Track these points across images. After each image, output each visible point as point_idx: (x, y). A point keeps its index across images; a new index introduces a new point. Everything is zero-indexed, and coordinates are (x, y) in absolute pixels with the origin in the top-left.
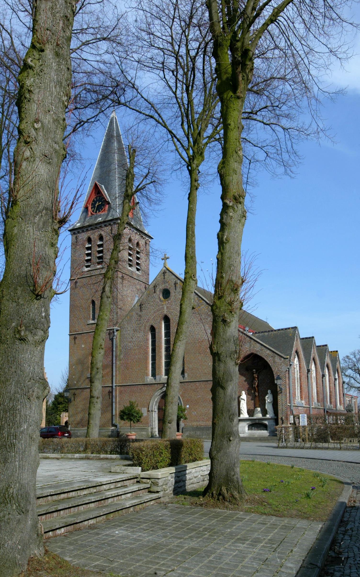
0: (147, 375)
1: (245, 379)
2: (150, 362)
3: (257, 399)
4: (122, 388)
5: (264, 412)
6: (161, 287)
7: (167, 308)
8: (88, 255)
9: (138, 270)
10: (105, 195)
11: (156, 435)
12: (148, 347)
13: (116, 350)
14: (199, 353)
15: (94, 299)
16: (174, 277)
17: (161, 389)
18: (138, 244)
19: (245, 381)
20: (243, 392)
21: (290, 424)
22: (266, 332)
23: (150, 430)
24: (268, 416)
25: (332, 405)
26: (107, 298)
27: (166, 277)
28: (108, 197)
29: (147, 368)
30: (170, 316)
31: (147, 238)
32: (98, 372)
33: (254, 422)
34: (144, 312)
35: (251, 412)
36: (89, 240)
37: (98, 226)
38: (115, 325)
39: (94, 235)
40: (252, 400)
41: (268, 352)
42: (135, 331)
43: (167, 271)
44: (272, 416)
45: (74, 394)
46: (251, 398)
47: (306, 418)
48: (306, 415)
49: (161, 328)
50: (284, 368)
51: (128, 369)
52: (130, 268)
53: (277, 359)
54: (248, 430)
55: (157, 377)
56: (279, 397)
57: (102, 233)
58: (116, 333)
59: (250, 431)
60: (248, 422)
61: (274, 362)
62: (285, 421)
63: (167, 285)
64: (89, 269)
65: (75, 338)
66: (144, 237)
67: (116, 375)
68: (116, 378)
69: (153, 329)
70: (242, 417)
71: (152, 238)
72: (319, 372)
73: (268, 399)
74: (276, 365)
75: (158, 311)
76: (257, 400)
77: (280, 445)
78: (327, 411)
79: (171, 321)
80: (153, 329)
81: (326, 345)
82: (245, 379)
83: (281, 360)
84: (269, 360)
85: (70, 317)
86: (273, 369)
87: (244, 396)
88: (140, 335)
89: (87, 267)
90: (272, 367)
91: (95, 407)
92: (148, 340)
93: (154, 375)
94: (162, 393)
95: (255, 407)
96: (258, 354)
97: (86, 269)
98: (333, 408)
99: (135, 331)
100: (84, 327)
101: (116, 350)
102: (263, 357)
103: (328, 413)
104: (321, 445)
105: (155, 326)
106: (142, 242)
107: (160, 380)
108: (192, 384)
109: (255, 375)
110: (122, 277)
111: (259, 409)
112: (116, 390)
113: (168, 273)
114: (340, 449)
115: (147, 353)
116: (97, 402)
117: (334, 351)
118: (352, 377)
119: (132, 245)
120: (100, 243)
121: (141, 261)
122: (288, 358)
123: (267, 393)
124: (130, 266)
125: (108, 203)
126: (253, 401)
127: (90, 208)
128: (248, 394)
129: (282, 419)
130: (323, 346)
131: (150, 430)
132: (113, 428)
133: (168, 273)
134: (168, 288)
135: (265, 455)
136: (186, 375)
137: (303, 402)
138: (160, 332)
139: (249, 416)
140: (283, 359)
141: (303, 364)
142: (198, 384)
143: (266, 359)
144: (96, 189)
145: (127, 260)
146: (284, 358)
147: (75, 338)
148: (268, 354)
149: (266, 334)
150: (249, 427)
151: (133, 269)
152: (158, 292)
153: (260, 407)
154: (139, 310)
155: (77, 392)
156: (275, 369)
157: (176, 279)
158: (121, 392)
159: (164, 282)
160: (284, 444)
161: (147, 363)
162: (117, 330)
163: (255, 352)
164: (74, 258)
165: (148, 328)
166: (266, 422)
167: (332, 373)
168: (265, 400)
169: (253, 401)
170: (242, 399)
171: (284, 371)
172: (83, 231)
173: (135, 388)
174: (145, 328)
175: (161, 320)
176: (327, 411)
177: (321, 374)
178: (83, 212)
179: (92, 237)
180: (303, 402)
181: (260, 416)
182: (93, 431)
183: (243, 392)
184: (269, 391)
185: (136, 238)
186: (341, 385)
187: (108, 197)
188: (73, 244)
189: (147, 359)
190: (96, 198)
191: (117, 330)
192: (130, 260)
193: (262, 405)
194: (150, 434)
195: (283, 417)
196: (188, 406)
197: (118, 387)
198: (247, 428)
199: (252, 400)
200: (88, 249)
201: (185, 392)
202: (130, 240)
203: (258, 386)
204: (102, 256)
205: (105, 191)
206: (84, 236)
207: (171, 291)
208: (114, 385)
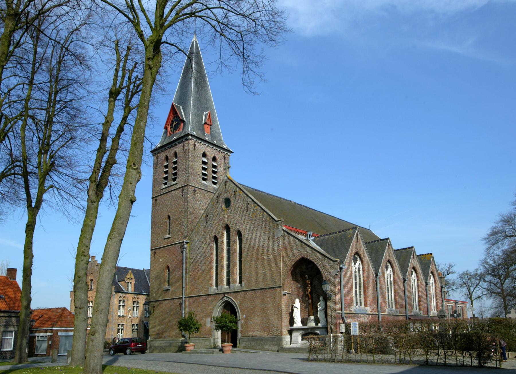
0: (211, 285)
1: (299, 286)
2: (215, 273)
3: (311, 306)
4: (191, 299)
5: (317, 321)
6: (223, 197)
7: (228, 217)
8: (166, 172)
9: (214, 183)
10: (181, 114)
11: (218, 346)
12: (212, 257)
13: (186, 262)
14: (255, 261)
15: (170, 214)
16: (234, 185)
17: (222, 299)
18: (214, 159)
19: (300, 288)
20: (297, 300)
21: (342, 333)
22: (327, 235)
23: (212, 341)
24: (319, 325)
25: (422, 312)
26: (92, 202)
27: (227, 186)
28: (184, 116)
29: (210, 278)
30: (230, 225)
31: (226, 153)
32: (79, 281)
33: (306, 332)
34: (209, 223)
35: (304, 321)
36: (167, 159)
37: (173, 144)
38: (185, 238)
39: (170, 153)
40: (306, 307)
41: (318, 255)
42: (201, 242)
43: (228, 180)
44: (323, 324)
45: (154, 307)
46: (305, 305)
47: (358, 326)
48: (357, 323)
50: (333, 272)
51: (195, 281)
52: (203, 182)
53: (326, 262)
54: (302, 340)
55: (219, 287)
56: (329, 304)
57: (177, 150)
58: (185, 246)
59: (303, 342)
60: (301, 332)
61: (324, 266)
62: (334, 330)
63: (228, 193)
64: (166, 186)
65: (155, 253)
66: (222, 151)
67: (186, 287)
68: (186, 290)
69: (216, 239)
71: (232, 152)
72: (399, 277)
73: (320, 306)
74: (327, 269)
75: (220, 220)
76: (310, 308)
77: (311, 358)
78: (409, 318)
79: (231, 230)
80: (216, 239)
81: (412, 247)
82: (299, 286)
83: (330, 263)
84: (319, 264)
85: (151, 234)
86: (323, 274)
87: (297, 304)
88: (205, 246)
89: (165, 184)
90: (321, 271)
91: (78, 318)
92: (212, 250)
93: (228, 283)
94: (223, 303)
95: (309, 316)
96: (308, 258)
97: (164, 187)
98: (422, 315)
99: (201, 242)
100: (161, 242)
101: (186, 262)
102: (313, 261)
103: (415, 319)
104: (378, 357)
105: (218, 236)
106: (219, 156)
107: (221, 290)
108: (248, 293)
109: (307, 281)
110: (194, 190)
112: (185, 302)
113: (229, 182)
114: (373, 362)
115: (211, 264)
116: (79, 313)
117: (428, 254)
118: (492, 283)
119: (208, 159)
120: (175, 160)
121: (219, 174)
122: (337, 261)
123: (319, 301)
124: (204, 179)
125: (183, 121)
126: (307, 309)
127: (169, 129)
128: (303, 301)
129: (331, 328)
130: (409, 248)
131: (212, 341)
132: (183, 339)
133: (229, 182)
134: (229, 197)
135: (255, 369)
136: (243, 283)
137: (367, 308)
138: (222, 242)
139: (303, 325)
140: (332, 262)
141: (369, 267)
143: (315, 263)
144: (173, 109)
145: (201, 175)
146: (334, 261)
147: (155, 253)
148: (318, 258)
149: (327, 237)
150: (302, 337)
151: (208, 183)
152: (220, 203)
153: (313, 315)
154: (205, 221)
155: (156, 304)
156: (324, 274)
157: (236, 187)
158: (189, 303)
159: (226, 191)
160: (329, 356)
161: (211, 273)
162: (187, 243)
163: (306, 257)
164: (155, 177)
165: (212, 238)
166: (318, 332)
168: (317, 308)
169: (307, 309)
170: (295, 307)
171: (333, 275)
172: (162, 151)
173: (200, 299)
174: (209, 239)
175: (223, 230)
176: (409, 318)
177: (401, 277)
178: (164, 134)
179: (168, 155)
180: (367, 308)
181: (312, 324)
182: (77, 343)
183: (297, 300)
185: (211, 152)
186: (439, 290)
187: (184, 116)
188: (154, 164)
189: (211, 269)
190: (174, 118)
191: (187, 243)
192: (204, 174)
193: (315, 314)
194: (212, 344)
195: (332, 326)
196: (244, 316)
197: (187, 299)
198: (300, 338)
199: (306, 307)
200: (166, 167)
201: (242, 302)
202: (204, 155)
203: (310, 293)
204: (176, 173)
205: (182, 110)
206: (162, 156)
207: (231, 200)
208: (184, 296)
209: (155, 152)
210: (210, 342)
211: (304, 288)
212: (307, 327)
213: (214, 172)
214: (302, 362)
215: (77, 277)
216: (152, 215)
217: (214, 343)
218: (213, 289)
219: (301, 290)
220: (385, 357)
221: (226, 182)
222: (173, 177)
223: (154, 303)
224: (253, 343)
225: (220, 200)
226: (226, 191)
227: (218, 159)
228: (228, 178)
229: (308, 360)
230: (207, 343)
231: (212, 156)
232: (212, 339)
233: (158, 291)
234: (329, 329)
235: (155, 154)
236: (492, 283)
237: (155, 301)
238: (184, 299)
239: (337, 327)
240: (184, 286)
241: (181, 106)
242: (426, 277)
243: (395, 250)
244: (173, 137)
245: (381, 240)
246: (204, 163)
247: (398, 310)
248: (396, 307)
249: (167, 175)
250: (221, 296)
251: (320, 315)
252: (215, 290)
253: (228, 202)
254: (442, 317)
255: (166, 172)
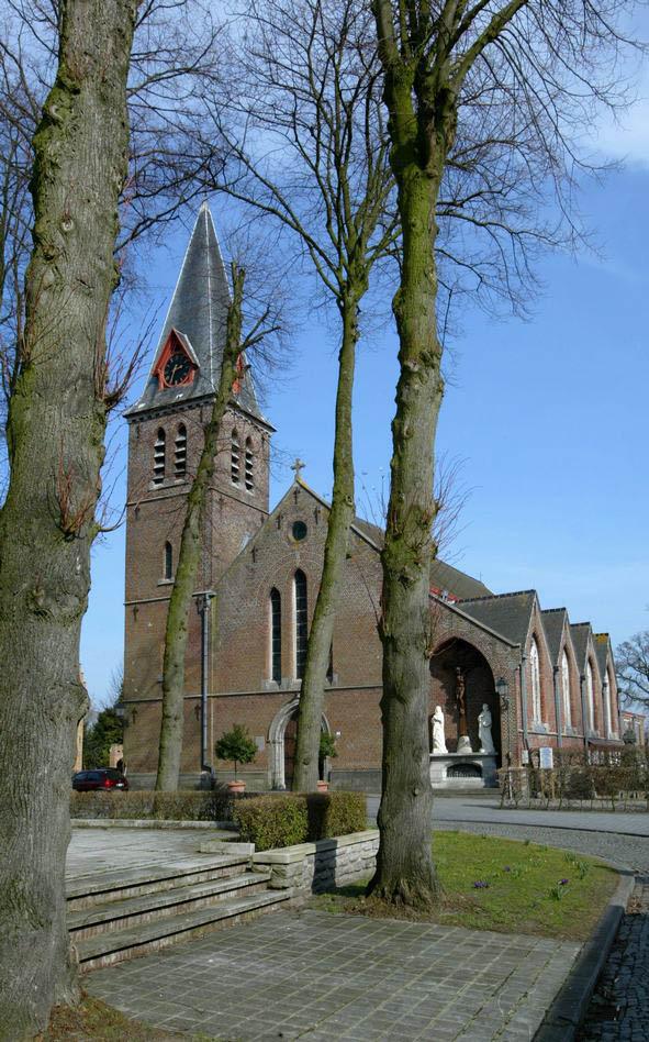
2: (271, 654)
4: (220, 701)
5: (476, 744)
6: (291, 518)
7: (301, 556)
8: (159, 460)
9: (249, 487)
18: (248, 441)
20: (439, 708)
23: (270, 777)
24: (483, 751)
29: (264, 664)
30: (306, 571)
34: (259, 563)
35: (451, 744)
38: (208, 587)
39: (170, 425)
40: (454, 721)
41: (484, 635)
42: (243, 597)
45: (134, 712)
49: (290, 594)
50: (512, 665)
51: (231, 667)
52: (234, 484)
53: (499, 647)
57: (185, 421)
58: (209, 602)
59: (451, 779)
62: (513, 760)
65: (135, 611)
67: (210, 678)
68: (210, 683)
69: (275, 595)
70: (436, 752)
71: (275, 431)
73: (484, 720)
74: (498, 659)
76: (463, 721)
79: (309, 580)
80: (275, 595)
81: (588, 624)
84: (485, 650)
86: (493, 667)
87: (439, 715)
89: (157, 481)
92: (266, 614)
93: (277, 677)
95: (460, 735)
96: (465, 638)
97: (156, 486)
102: (474, 644)
103: (591, 745)
104: (577, 803)
105: (279, 588)
106: (256, 438)
111: (467, 739)
112: (209, 705)
114: (613, 810)
115: (265, 638)
118: (634, 681)
119: (239, 442)
120: (180, 439)
123: (482, 710)
124: (235, 480)
125: (196, 367)
127: (162, 376)
128: (447, 712)
130: (582, 624)
131: (270, 777)
137: (546, 725)
138: (290, 600)
140: (509, 649)
142: (356, 693)
144: (173, 342)
145: (230, 470)
146: (513, 647)
148: (483, 639)
149: (480, 602)
150: (448, 771)
151: (240, 486)
155: (138, 708)
157: (318, 504)
158: (218, 708)
159: (297, 509)
162: (211, 597)
165: (267, 593)
166: (480, 762)
167: (598, 673)
172: (150, 418)
173: (244, 701)
175: (290, 579)
180: (546, 725)
181: (468, 750)
183: (439, 708)
184: (485, 707)
185: (245, 429)
186: (614, 696)
188: (131, 441)
189: (265, 648)
191: (211, 597)
193: (473, 730)
196: (338, 733)
197: (212, 700)
198: (444, 774)
199: (454, 721)
200: (159, 449)
202: (235, 434)
206: (151, 426)
207: (308, 526)
208: (206, 695)
209: (134, 417)
210: (266, 779)
211: (452, 690)
212: (455, 754)
213: (249, 467)
214: (491, 810)
215: (72, 657)
216: (127, 538)
217: (198, 788)
218: (270, 683)
219: (443, 692)
220: (587, 803)
221: (296, 493)
222: (177, 471)
223: (134, 706)
224: (358, 781)
225: (284, 523)
226: (297, 509)
227: (254, 442)
228: (301, 486)
229: (501, 807)
230: (260, 782)
231: (246, 436)
232: (270, 773)
233: (144, 681)
234: (504, 758)
235: (134, 421)
236: (634, 681)
237: (138, 702)
238: (206, 700)
239: (517, 755)
240: (206, 676)
241: (186, 336)
242: (582, 667)
243: (572, 625)
244: (173, 394)
245: (496, 597)
246: (235, 449)
247: (575, 729)
248: (573, 723)
249: (161, 465)
250: (289, 698)
251: (484, 734)
252: (273, 685)
253: (300, 530)
254: (630, 742)
255: (159, 460)
